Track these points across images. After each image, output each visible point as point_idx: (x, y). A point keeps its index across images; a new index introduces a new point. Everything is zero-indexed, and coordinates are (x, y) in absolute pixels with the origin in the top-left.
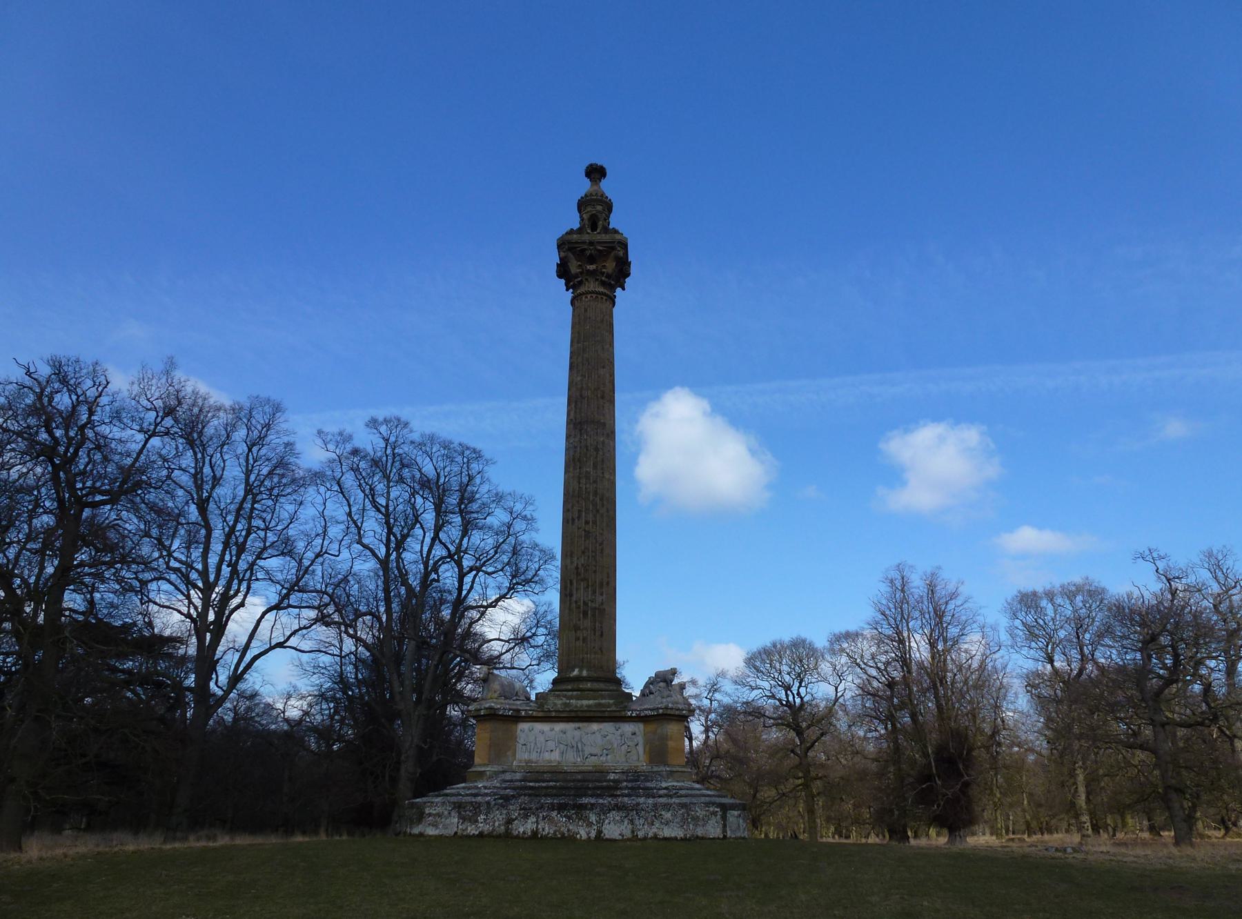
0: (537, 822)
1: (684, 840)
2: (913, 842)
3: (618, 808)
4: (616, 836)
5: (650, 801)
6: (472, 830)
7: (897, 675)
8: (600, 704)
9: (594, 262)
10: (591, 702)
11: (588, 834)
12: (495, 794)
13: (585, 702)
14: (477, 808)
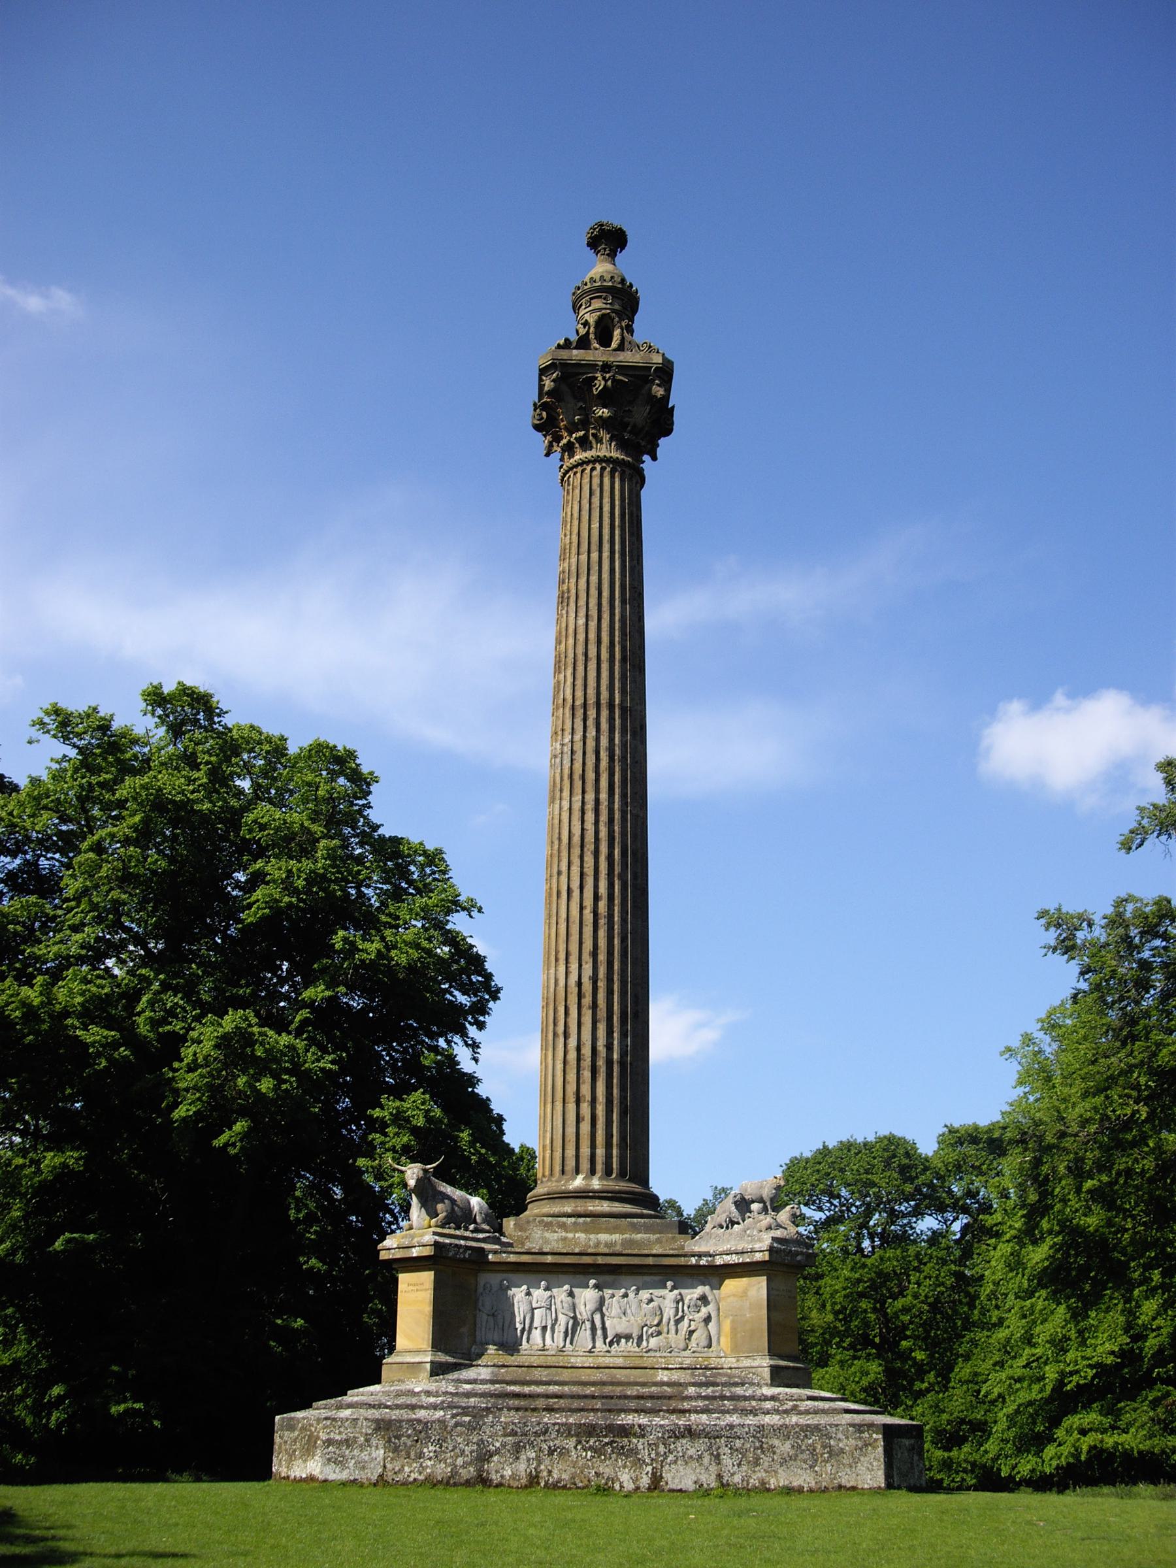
0: (539, 1461)
1: (344, 1484)
2: (150, 1504)
3: (690, 1433)
4: (688, 1484)
5: (750, 1420)
6: (411, 1471)
7: (268, 878)
8: (631, 1242)
9: (608, 407)
10: (616, 1237)
11: (635, 1480)
12: (451, 1406)
13: (604, 1237)
14: (422, 1430)
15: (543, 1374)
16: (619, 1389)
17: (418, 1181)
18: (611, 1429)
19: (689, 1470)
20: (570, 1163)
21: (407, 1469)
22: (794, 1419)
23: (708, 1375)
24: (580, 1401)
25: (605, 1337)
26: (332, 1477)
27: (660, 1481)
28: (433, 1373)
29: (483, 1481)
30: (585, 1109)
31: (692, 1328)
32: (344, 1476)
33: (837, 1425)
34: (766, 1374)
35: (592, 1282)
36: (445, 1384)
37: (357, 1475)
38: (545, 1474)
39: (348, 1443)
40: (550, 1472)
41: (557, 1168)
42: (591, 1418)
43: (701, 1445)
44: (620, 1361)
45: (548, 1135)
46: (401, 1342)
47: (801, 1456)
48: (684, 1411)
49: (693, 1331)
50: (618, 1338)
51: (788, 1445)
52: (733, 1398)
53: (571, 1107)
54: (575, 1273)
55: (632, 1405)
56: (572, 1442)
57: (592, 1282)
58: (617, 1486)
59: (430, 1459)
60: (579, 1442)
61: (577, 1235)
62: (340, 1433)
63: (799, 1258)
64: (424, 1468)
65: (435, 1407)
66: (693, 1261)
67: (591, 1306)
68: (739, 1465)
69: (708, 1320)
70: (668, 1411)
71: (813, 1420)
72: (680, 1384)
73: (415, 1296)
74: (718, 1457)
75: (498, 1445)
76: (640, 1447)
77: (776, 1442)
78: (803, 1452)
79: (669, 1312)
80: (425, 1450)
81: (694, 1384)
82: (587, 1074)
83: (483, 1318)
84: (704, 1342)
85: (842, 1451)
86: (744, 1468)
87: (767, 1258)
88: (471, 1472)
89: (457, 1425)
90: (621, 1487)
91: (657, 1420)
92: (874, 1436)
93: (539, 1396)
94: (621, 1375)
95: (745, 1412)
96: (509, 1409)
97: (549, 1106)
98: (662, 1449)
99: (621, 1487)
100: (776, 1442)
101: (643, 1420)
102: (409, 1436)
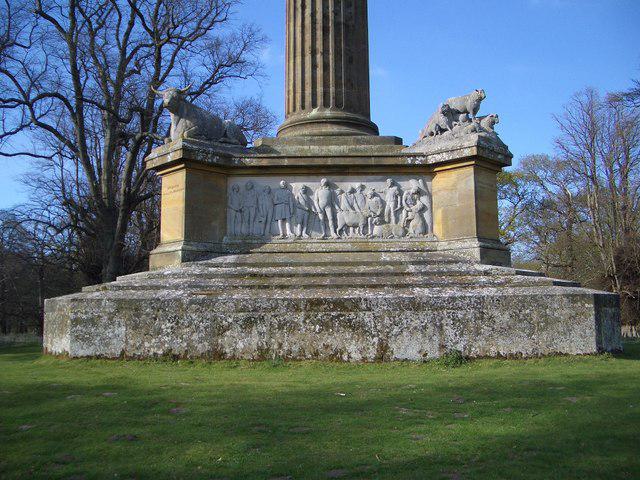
3: (416, 306)
6: (152, 346)
15: (281, 258)
16: (347, 268)
17: (173, 98)
18: (339, 304)
19: (414, 342)
20: (308, 99)
21: (147, 344)
22: (511, 291)
23: (424, 257)
24: (311, 281)
25: (336, 227)
26: (81, 353)
27: (385, 351)
28: (185, 259)
29: (217, 355)
30: (319, 58)
31: (409, 218)
32: (89, 351)
33: (552, 296)
34: (477, 256)
35: (324, 180)
36: (195, 269)
37: (101, 351)
38: (276, 347)
39: (93, 322)
40: (280, 345)
41: (298, 105)
42: (320, 294)
43: (424, 317)
44: (349, 246)
45: (292, 82)
46: (165, 235)
47: (519, 325)
48: (407, 286)
49: (410, 220)
50: (346, 227)
51: (506, 317)
52: (451, 274)
53: (308, 58)
54: (309, 174)
55: (359, 281)
56: (300, 317)
57: (324, 180)
58: (345, 358)
59: (168, 335)
60: (308, 317)
61: (312, 147)
62: (86, 313)
63: (499, 157)
64: (163, 343)
65: (177, 287)
66: (409, 161)
67: (323, 201)
68: (461, 335)
69: (423, 209)
70: (393, 286)
71: (530, 291)
72: (401, 263)
73: (173, 193)
74: (441, 327)
75: (230, 320)
76: (367, 320)
77: (496, 313)
78: (520, 321)
79: (390, 204)
80: (163, 327)
81: (413, 263)
82: (319, 33)
83: (232, 213)
84: (419, 229)
85: (557, 320)
86: (466, 337)
87: (475, 153)
88: (203, 347)
89: (192, 302)
90: (349, 357)
91: (381, 294)
92: (586, 305)
93: (274, 275)
94: (350, 257)
95: (464, 286)
96: (244, 287)
97: (292, 24)
98: (387, 321)
99: (349, 357)
100: (496, 313)
101: (369, 294)
102: (148, 315)
